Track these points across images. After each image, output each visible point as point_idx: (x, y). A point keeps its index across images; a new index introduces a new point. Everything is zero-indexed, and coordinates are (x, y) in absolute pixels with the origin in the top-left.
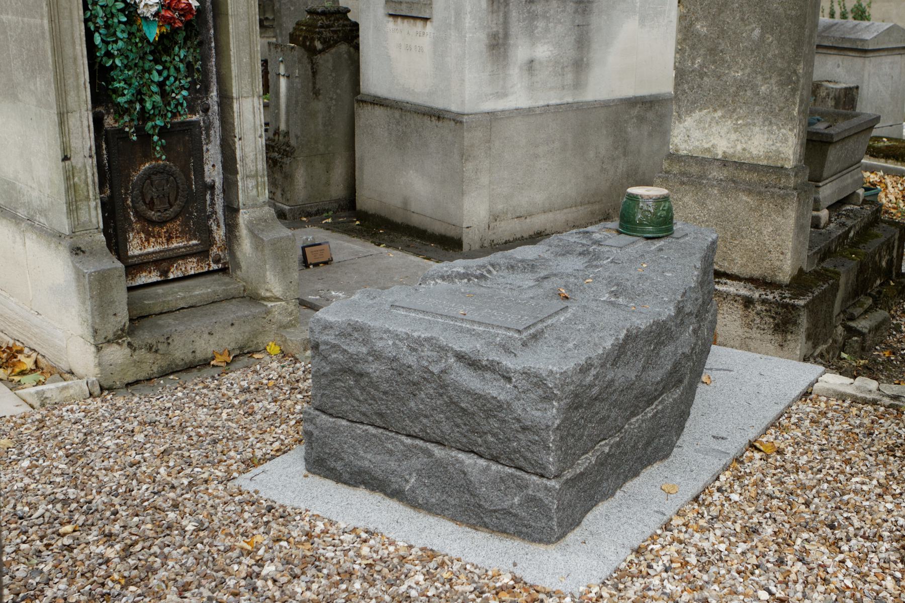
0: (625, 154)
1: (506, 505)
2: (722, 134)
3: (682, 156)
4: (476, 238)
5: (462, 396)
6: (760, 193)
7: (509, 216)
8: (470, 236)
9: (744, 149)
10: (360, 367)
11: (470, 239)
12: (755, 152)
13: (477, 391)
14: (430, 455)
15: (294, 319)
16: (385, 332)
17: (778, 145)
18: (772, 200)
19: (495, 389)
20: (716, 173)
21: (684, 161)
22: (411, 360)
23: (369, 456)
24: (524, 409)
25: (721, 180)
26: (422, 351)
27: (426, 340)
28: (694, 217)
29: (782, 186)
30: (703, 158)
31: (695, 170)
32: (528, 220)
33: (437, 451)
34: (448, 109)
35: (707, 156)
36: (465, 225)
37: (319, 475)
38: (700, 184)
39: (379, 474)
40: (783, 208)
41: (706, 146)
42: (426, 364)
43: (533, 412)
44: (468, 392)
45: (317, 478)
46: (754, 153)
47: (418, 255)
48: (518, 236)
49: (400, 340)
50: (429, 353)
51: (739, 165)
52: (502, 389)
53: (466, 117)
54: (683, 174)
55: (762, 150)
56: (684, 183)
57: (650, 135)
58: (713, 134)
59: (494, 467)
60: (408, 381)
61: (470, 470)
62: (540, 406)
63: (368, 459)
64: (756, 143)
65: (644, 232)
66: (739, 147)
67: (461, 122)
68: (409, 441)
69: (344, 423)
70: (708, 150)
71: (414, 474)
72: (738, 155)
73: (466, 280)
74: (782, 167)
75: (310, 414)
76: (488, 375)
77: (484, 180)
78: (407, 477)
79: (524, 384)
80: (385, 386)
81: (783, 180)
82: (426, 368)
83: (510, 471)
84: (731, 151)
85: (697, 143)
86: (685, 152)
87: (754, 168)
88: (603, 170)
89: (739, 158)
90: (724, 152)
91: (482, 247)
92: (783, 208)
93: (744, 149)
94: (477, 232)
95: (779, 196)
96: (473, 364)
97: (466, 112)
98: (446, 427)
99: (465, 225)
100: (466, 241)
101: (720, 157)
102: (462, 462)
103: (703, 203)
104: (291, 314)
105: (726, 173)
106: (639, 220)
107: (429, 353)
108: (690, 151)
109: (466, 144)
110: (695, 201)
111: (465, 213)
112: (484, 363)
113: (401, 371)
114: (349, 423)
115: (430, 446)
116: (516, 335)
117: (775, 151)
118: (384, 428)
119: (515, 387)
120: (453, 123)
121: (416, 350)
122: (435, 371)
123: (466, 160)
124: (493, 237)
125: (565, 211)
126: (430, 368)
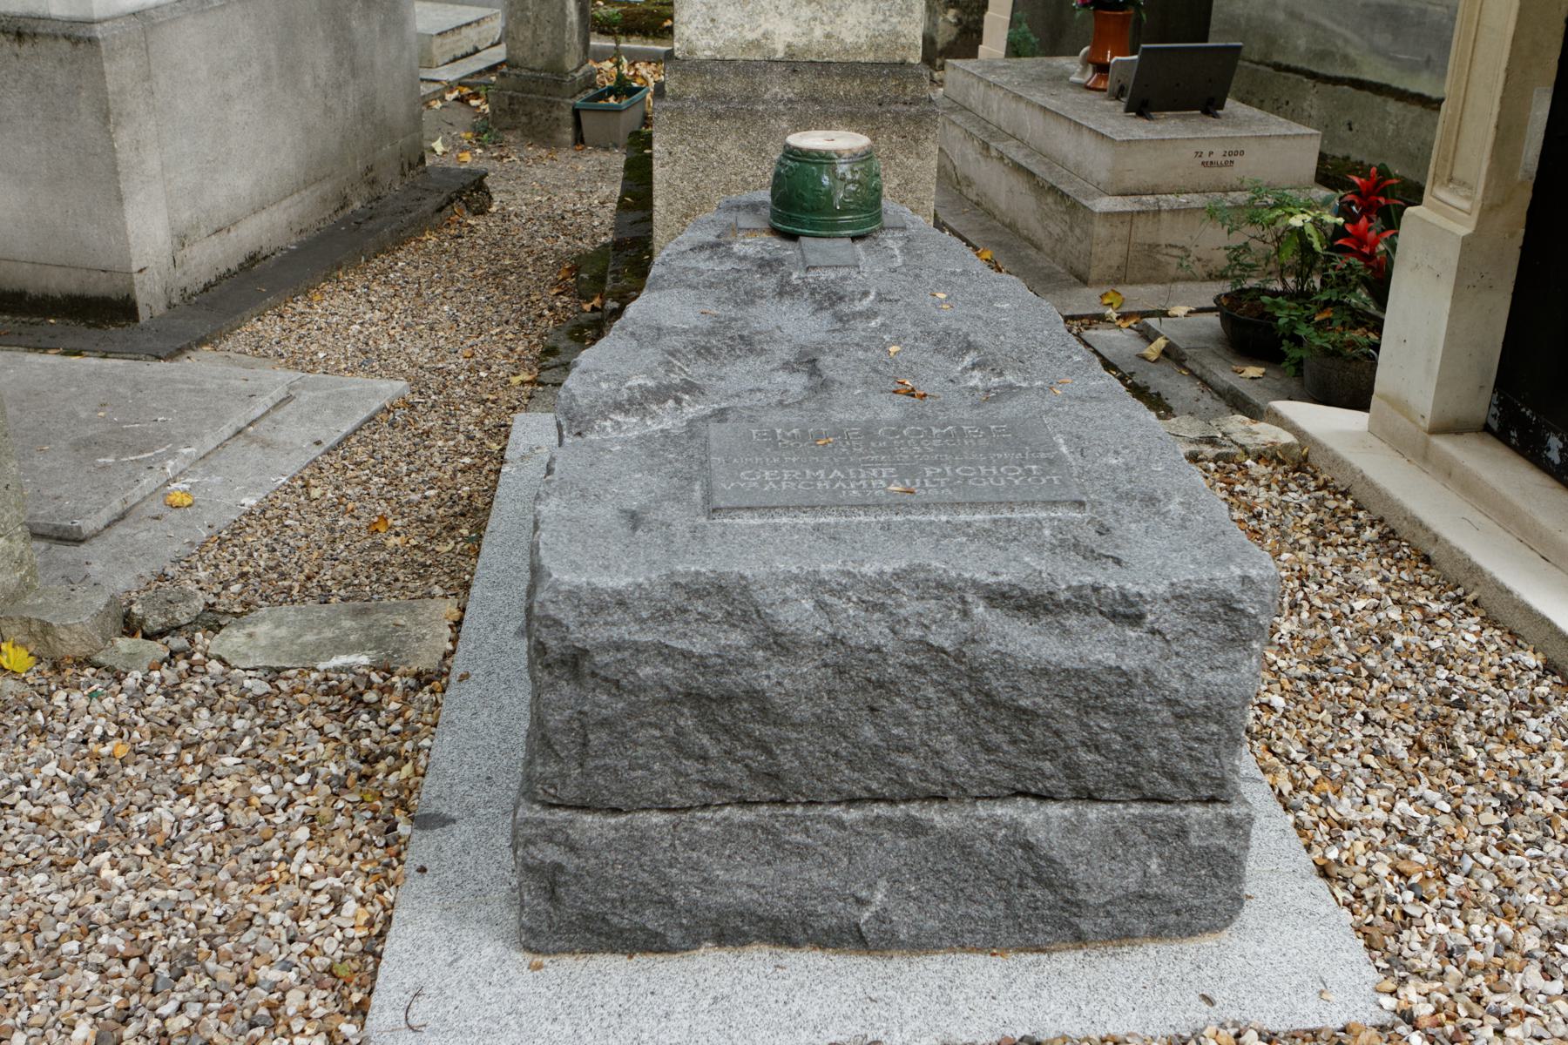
0: (354, 73)
1: (1132, 882)
2: (782, 9)
3: (702, 62)
4: (158, 290)
5: (1023, 683)
6: (872, 117)
7: (203, 231)
8: (147, 288)
9: (828, 36)
10: (734, 681)
11: (150, 295)
12: (850, 39)
13: (1068, 664)
14: (916, 828)
15: (29, 573)
16: (787, 583)
17: (894, 20)
18: (896, 128)
19: (1100, 648)
20: (777, 89)
21: (712, 72)
22: (878, 632)
23: (743, 875)
24: (1187, 676)
25: (790, 100)
26: (900, 606)
27: (897, 575)
28: (744, 180)
29: (908, 98)
30: (747, 62)
31: (734, 86)
32: (233, 234)
33: (935, 816)
34: (41, 12)
35: (756, 56)
36: (135, 268)
37: (571, 952)
38: (752, 112)
39: (780, 908)
40: (916, 141)
41: (750, 36)
42: (918, 633)
43: (1209, 676)
44: (1042, 672)
45: (567, 960)
46: (848, 41)
47: (43, 349)
48: (223, 270)
49: (832, 592)
50: (918, 606)
51: (823, 68)
52: (1123, 643)
53: (98, 27)
54: (710, 97)
55: (863, 33)
56: (719, 116)
57: (384, 31)
58: (763, 11)
59: (1094, 812)
60: (860, 676)
61: (1041, 835)
62: (1220, 658)
63: (743, 882)
64: (851, 21)
65: (843, 227)
66: (818, 33)
67: (91, 41)
68: (853, 815)
69: (657, 818)
70: (756, 44)
71: (883, 884)
72: (816, 48)
73: (671, 403)
74: (902, 63)
75: (543, 822)
76: (1073, 621)
77: (153, 163)
78: (864, 894)
79: (1170, 620)
80: (804, 711)
81: (910, 87)
82: (920, 641)
83: (1136, 809)
84: (801, 42)
85: (732, 33)
86: (708, 53)
87: (851, 70)
88: (328, 111)
89: (819, 54)
90: (789, 46)
91: (170, 306)
92: (916, 141)
93: (828, 36)
94: (157, 277)
95: (909, 118)
96: (1030, 604)
97: (96, 16)
98: (957, 759)
99: (135, 268)
100: (141, 299)
101: (780, 55)
102: (1015, 826)
103: (761, 150)
104: (20, 562)
105: (798, 87)
106: (842, 202)
107: (918, 606)
108: (719, 50)
109: (110, 88)
110: (742, 148)
111: (131, 240)
112: (1062, 596)
113: (848, 664)
114: (667, 816)
115: (914, 809)
116: (1075, 515)
117: (889, 33)
118: (773, 802)
119: (1153, 632)
120: (65, 46)
121: (881, 607)
122: (947, 645)
123: (117, 124)
124: (184, 282)
125: (285, 203)
126: (932, 639)
